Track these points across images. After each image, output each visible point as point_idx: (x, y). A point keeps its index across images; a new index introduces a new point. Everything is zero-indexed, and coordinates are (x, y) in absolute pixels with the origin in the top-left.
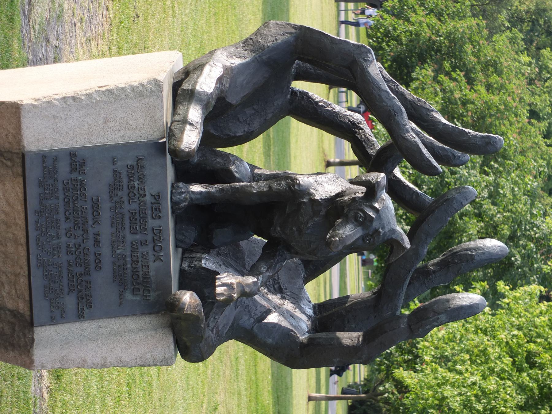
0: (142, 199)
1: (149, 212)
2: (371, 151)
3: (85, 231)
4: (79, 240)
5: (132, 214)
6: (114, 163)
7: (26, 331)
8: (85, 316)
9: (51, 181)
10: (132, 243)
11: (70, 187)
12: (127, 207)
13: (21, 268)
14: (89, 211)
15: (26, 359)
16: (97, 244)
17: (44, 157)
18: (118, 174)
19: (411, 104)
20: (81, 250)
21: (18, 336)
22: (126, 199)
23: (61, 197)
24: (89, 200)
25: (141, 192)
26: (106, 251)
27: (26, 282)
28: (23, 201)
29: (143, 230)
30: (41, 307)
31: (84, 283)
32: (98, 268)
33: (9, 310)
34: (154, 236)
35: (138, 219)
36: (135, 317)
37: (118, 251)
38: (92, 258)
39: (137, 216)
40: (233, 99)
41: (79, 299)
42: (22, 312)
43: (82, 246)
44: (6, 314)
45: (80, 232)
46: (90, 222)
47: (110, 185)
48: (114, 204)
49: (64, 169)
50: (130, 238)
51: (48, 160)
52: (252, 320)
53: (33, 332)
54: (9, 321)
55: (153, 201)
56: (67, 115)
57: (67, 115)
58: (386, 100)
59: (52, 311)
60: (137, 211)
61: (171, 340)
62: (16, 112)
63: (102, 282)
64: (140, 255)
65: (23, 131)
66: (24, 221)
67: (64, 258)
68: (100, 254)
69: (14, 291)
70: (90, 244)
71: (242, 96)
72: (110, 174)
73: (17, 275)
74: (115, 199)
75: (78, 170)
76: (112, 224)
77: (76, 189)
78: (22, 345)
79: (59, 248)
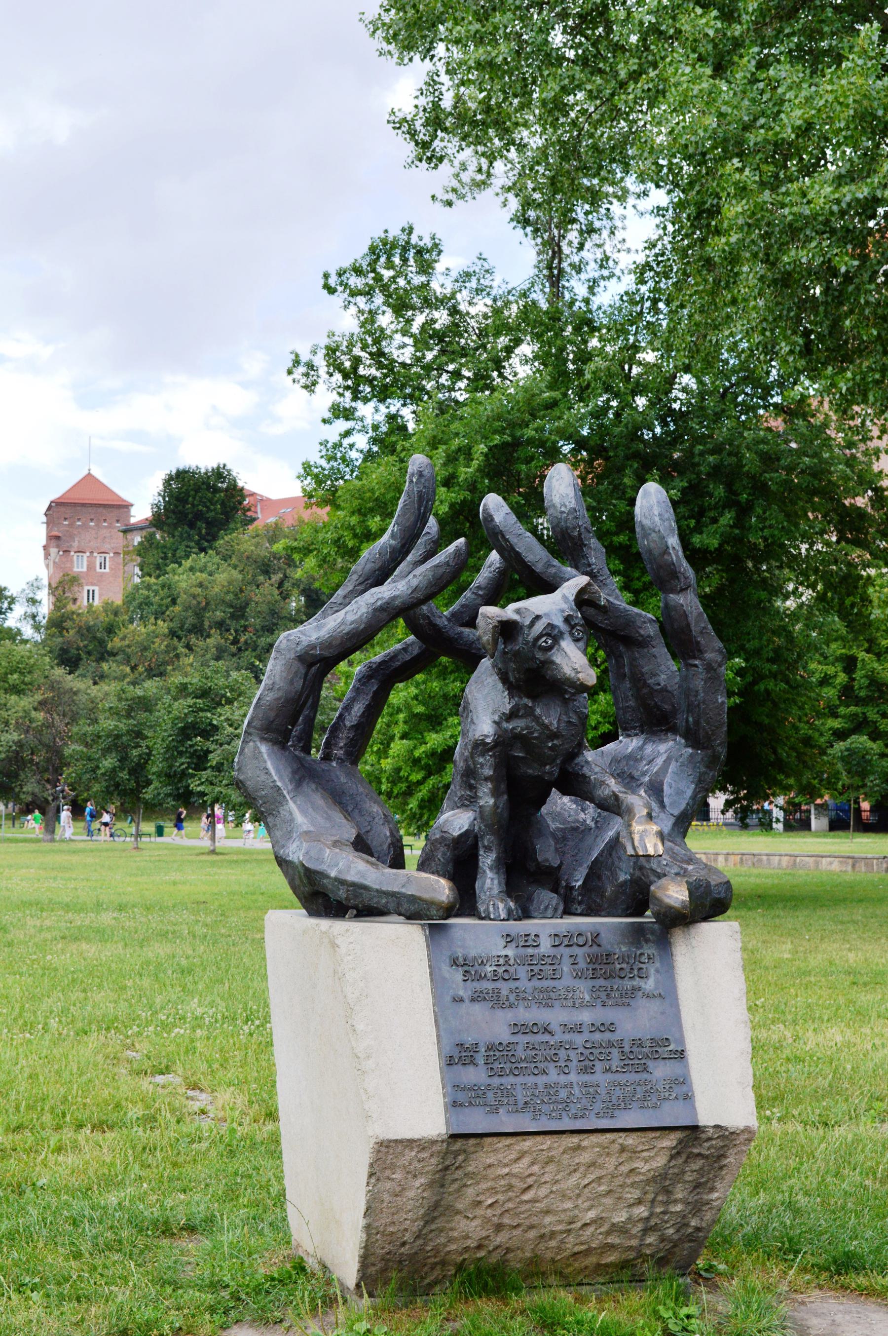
0: (512, 962)
1: (530, 951)
2: (416, 651)
3: (561, 1045)
4: (573, 1055)
8: (680, 1049)
9: (490, 1095)
13: (613, 1141)
14: (529, 1038)
15: (742, 1138)
16: (578, 1029)
17: (454, 1105)
19: (360, 584)
20: (587, 1052)
21: (709, 1149)
22: (512, 984)
23: (511, 1079)
24: (514, 1039)
25: (502, 961)
26: (586, 1017)
27: (634, 1135)
28: (519, 1138)
30: (671, 1114)
31: (635, 1049)
32: (610, 1028)
33: (669, 1161)
37: (587, 997)
40: (351, 833)
42: (675, 1143)
45: (562, 1053)
46: (546, 1037)
49: (475, 1075)
50: (567, 981)
53: (705, 1127)
54: (686, 1162)
55: (514, 944)
58: (359, 614)
61: (705, 927)
62: (387, 1147)
63: (636, 1022)
66: (547, 1137)
67: (600, 1077)
69: (645, 1154)
71: (344, 821)
72: (477, 1007)
73: (623, 1149)
76: (548, 1006)
77: (498, 1056)
79: (586, 1085)
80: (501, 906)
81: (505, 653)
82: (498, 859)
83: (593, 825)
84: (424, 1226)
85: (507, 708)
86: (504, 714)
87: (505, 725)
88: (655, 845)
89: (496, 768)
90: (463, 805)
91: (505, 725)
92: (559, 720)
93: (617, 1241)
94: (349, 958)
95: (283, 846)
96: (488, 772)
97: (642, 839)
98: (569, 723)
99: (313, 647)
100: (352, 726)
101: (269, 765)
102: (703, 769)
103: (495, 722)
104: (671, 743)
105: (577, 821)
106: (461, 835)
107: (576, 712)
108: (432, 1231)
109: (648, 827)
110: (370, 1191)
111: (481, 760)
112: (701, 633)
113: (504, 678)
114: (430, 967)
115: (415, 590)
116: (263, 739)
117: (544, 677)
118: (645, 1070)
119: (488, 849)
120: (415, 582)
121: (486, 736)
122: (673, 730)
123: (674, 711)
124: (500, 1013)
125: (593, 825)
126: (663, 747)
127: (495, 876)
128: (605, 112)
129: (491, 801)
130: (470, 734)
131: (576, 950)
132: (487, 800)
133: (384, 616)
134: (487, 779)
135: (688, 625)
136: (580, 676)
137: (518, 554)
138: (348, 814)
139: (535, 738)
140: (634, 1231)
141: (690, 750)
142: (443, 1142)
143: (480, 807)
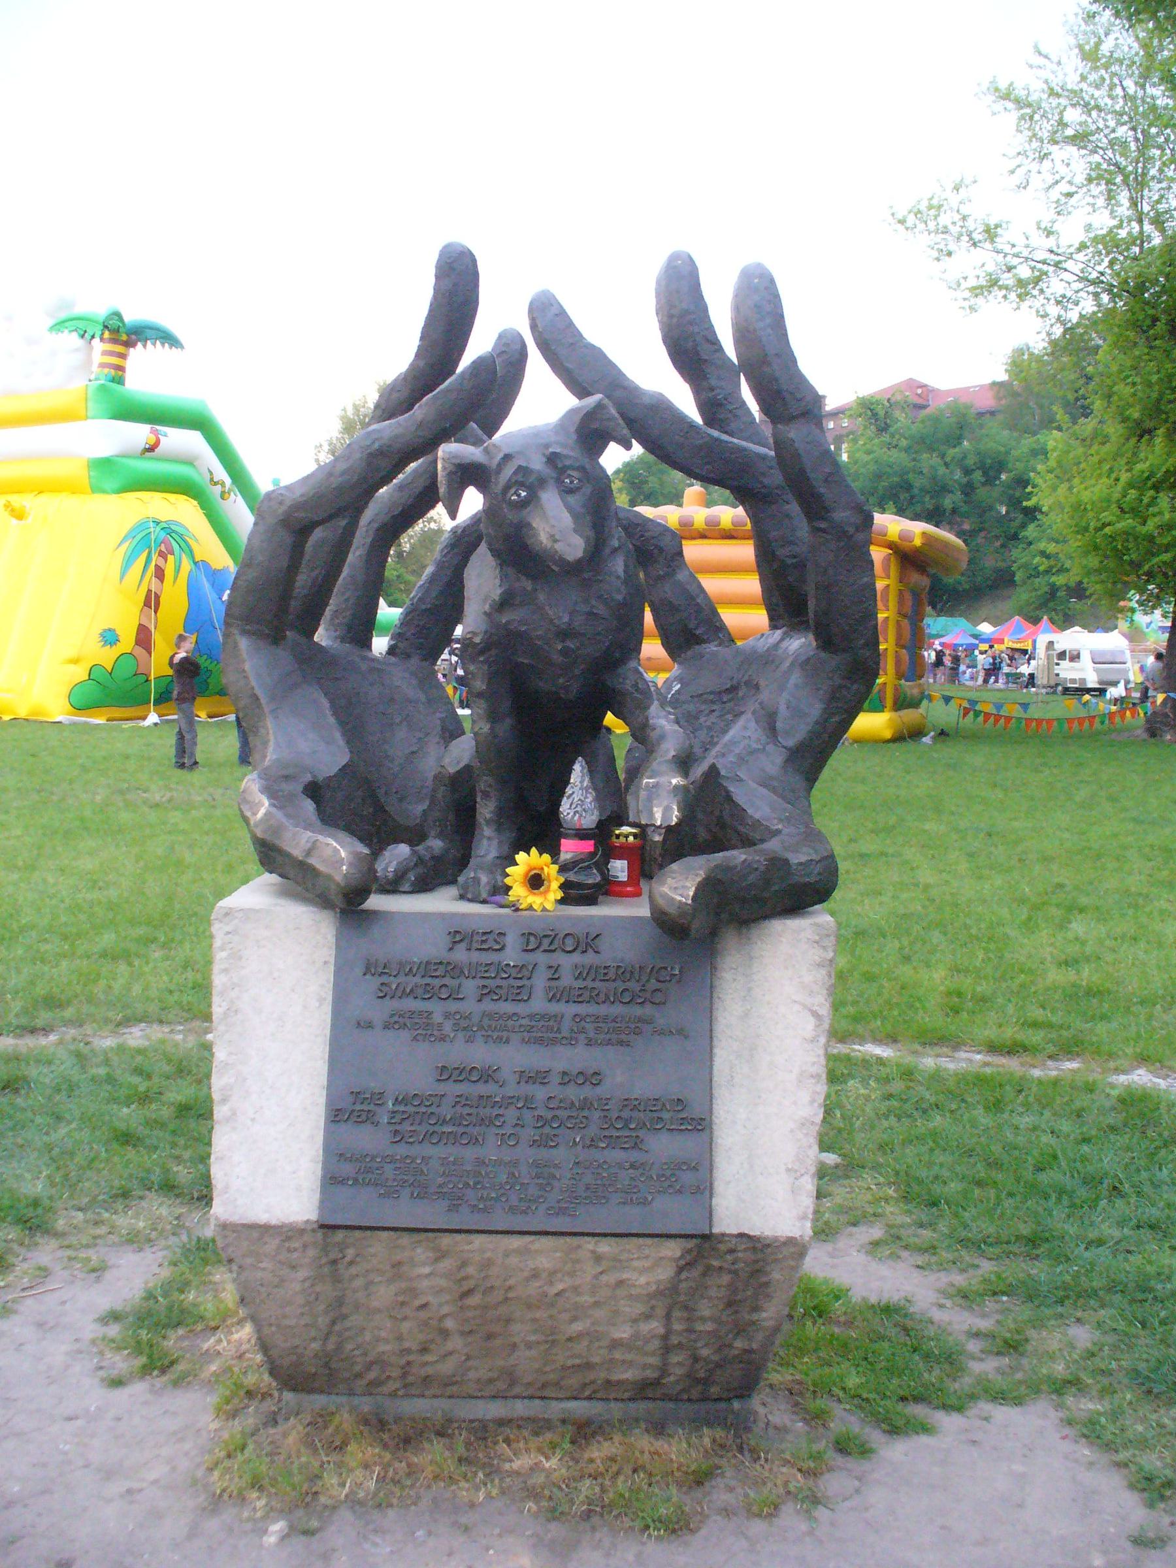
3: (509, 1101)
4: (528, 1116)
5: (485, 994)
6: (370, 1025)
7: (722, 1247)
10: (550, 1001)
11: (406, 1127)
12: (470, 1006)
13: (579, 1247)
14: (460, 1089)
15: (786, 1251)
16: (539, 1077)
17: (331, 1181)
18: (396, 1018)
22: (453, 1006)
24: (442, 1088)
29: (523, 972)
30: (672, 1212)
32: (593, 1078)
34: (542, 949)
35: (499, 982)
36: (717, 1004)
38: (573, 1093)
41: (656, 1125)
42: (678, 1254)
44: (687, 1279)
45: (511, 1115)
47: (415, 1039)
48: (460, 1035)
49: (369, 1139)
51: (342, 1171)
52: (770, 748)
55: (463, 945)
56: (253, 1120)
57: (253, 1120)
59: (680, 1192)
63: (629, 1075)
64: (580, 984)
65: (274, 1222)
68: (565, 1073)
70: (540, 1093)
74: (448, 1028)
75: (372, 1107)
77: (414, 1115)
78: (753, 1257)
89: (491, 678)
94: (224, 954)
98: (591, 614)
99: (298, 506)
101: (247, 667)
102: (838, 681)
103: (485, 613)
104: (803, 640)
112: (826, 481)
113: (496, 553)
116: (244, 632)
117: (525, 547)
118: (635, 1146)
119: (486, 795)
124: (424, 1046)
131: (560, 958)
133: (385, 464)
136: (558, 547)
139: (539, 637)
140: (650, 1347)
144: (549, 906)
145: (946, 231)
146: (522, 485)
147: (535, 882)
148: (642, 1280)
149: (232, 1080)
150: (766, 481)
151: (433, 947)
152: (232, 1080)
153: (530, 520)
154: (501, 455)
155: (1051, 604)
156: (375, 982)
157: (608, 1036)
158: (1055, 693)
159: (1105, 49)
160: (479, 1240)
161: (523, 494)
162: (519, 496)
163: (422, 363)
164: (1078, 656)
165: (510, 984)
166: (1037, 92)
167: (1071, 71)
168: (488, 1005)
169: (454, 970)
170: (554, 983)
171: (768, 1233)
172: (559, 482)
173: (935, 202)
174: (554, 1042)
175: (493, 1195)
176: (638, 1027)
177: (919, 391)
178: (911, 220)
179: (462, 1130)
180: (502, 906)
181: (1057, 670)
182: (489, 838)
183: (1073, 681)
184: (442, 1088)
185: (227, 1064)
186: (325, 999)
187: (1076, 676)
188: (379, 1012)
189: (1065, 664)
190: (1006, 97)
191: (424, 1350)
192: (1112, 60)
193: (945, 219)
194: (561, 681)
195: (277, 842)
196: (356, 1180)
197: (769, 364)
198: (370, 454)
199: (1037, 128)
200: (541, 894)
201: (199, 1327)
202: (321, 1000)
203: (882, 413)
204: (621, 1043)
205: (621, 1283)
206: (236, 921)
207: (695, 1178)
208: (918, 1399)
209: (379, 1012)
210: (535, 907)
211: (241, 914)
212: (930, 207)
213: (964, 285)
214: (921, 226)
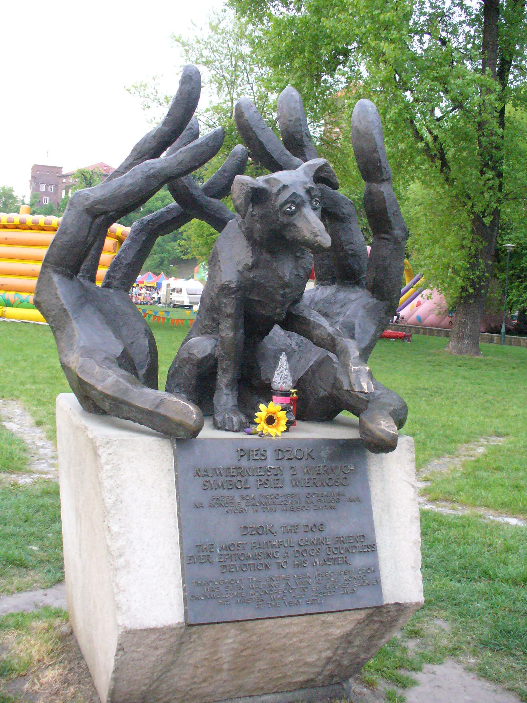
3: (281, 544)
4: (290, 551)
9: (222, 588)
12: (253, 492)
14: (254, 539)
16: (293, 529)
17: (190, 598)
22: (244, 492)
29: (277, 472)
30: (367, 599)
32: (320, 527)
34: (286, 458)
39: (263, 479)
40: (118, 349)
43: (297, 548)
49: (210, 572)
56: (139, 566)
57: (139, 566)
60: (258, 478)
63: (340, 525)
65: (159, 626)
70: (295, 538)
71: (113, 338)
74: (243, 504)
77: (232, 555)
80: (235, 419)
81: (253, 215)
82: (233, 380)
83: (296, 348)
84: (162, 675)
85: (249, 261)
86: (247, 265)
87: (246, 274)
88: (368, 384)
89: (237, 307)
90: (206, 333)
91: (246, 274)
92: (291, 273)
93: (306, 669)
94: (109, 467)
95: (66, 356)
96: (229, 310)
97: (357, 378)
99: (97, 202)
100: (127, 264)
101: (59, 292)
102: (382, 315)
103: (239, 271)
105: (285, 345)
106: (205, 358)
107: (303, 267)
108: (167, 677)
109: (362, 368)
110: (118, 659)
111: (225, 301)
112: (394, 214)
113: (250, 236)
114: (176, 477)
115: (180, 163)
116: (55, 271)
119: (225, 371)
120: (180, 158)
121: (231, 282)
122: (358, 283)
123: (361, 272)
124: (231, 517)
125: (296, 348)
126: (353, 296)
127: (230, 393)
128: (246, 30)
129: (231, 334)
130: (218, 279)
132: (227, 332)
134: (228, 316)
135: (385, 208)
136: (318, 239)
137: (261, 143)
138: (117, 332)
139: (271, 287)
141: (375, 301)
142: (181, 628)
143: (222, 338)
144: (279, 434)
145: (148, 97)
146: (293, 202)
147: (270, 420)
148: (338, 631)
149: (125, 543)
150: (344, 210)
151: (228, 459)
152: (125, 543)
153: (295, 222)
154: (281, 185)
155: (161, 267)
156: (200, 481)
157: (325, 504)
158: (169, 306)
159: (221, 26)
160: (268, 622)
161: (293, 208)
162: (291, 208)
163: (166, 129)
164: (181, 290)
165: (269, 479)
166: (192, 41)
167: (206, 33)
168: (262, 491)
169: (243, 472)
170: (294, 477)
171: (408, 601)
172: (311, 204)
173: (144, 84)
174: (298, 509)
175: (279, 597)
176: (338, 498)
177: (105, 168)
178: (133, 90)
179: (259, 562)
180: (249, 434)
181: (171, 296)
182: (227, 395)
183: (178, 302)
184: (246, 539)
185: (119, 533)
186: (172, 491)
187: (180, 299)
188: (205, 498)
189: (175, 294)
190: (178, 41)
191: (205, 680)
192: (224, 31)
193: (148, 92)
194: (278, 310)
195: (125, 399)
196: (205, 596)
197: (378, 152)
198: (148, 177)
199: (190, 56)
200: (273, 427)
201: (14, 676)
202: (169, 492)
203: (89, 177)
204: (331, 508)
205: (328, 634)
206: (114, 447)
207: (371, 577)
208: (401, 667)
209: (205, 498)
210: (272, 434)
211: (116, 443)
212: (141, 86)
213: (154, 121)
214: (137, 93)
